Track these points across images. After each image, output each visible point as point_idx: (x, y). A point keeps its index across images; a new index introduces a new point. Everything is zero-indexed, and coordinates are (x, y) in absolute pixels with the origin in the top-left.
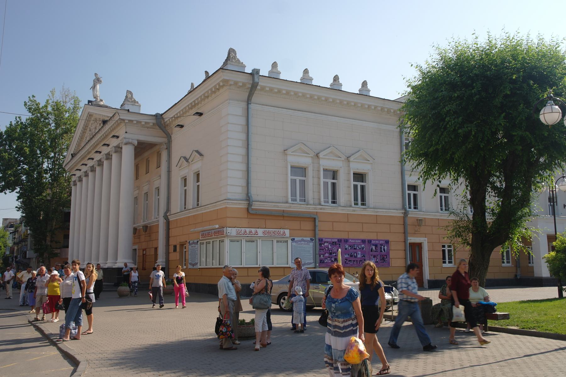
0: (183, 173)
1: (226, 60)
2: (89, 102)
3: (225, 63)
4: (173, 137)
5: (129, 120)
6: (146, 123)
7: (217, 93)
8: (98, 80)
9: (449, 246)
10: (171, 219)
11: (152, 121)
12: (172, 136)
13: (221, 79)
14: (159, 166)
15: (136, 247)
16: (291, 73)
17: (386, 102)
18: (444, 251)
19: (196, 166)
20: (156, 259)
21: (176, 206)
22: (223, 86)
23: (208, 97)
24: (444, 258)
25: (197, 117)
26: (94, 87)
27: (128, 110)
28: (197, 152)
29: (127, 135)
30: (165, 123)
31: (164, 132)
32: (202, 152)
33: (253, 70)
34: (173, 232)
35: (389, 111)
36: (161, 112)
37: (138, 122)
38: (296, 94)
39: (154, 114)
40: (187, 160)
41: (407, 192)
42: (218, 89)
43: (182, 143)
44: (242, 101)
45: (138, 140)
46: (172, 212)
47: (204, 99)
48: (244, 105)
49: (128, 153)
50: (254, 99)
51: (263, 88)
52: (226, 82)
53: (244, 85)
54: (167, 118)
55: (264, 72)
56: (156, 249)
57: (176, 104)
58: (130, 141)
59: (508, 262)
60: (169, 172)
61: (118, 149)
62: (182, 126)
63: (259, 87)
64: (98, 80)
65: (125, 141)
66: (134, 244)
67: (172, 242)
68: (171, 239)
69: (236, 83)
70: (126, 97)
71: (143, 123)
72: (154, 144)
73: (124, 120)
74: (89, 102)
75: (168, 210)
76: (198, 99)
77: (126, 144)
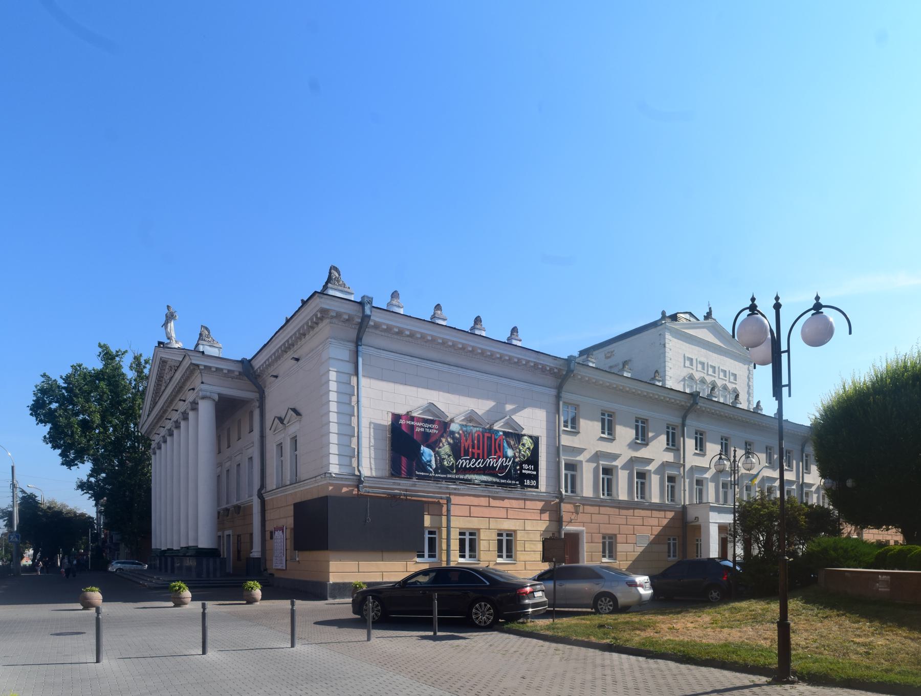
0: (279, 438)
1: (327, 283)
2: (160, 343)
3: (325, 287)
4: (267, 392)
5: (205, 366)
6: (229, 371)
7: (316, 329)
8: (170, 317)
9: (674, 539)
10: (267, 498)
11: (237, 368)
12: (266, 390)
13: (317, 308)
14: (251, 431)
15: (220, 533)
16: (415, 306)
17: (542, 357)
18: (604, 543)
19: (292, 429)
20: (252, 548)
21: (271, 483)
22: (322, 319)
23: (304, 335)
24: (604, 552)
25: (294, 362)
26: (165, 325)
27: (203, 352)
28: (294, 410)
29: (203, 386)
30: (255, 372)
31: (254, 384)
32: (301, 411)
33: (363, 297)
34: (268, 516)
35: (543, 369)
36: (249, 358)
37: (218, 370)
38: (423, 337)
39: (240, 359)
40: (281, 420)
41: (563, 472)
42: (317, 324)
43: (278, 400)
44: (348, 341)
45: (219, 394)
46: (269, 488)
47: (300, 339)
48: (352, 346)
49: (206, 410)
50: (366, 339)
51: (377, 326)
52: (324, 312)
53: (349, 320)
54: (257, 364)
55: (381, 301)
56: (251, 534)
57: (265, 345)
58: (208, 394)
59: (674, 556)
60: (262, 437)
61: (194, 406)
62: (276, 377)
63: (371, 323)
64: (170, 317)
65: (201, 394)
66: (219, 530)
67: (269, 527)
68: (267, 523)
69: (338, 315)
70: (201, 335)
71: (225, 371)
72: (243, 399)
73: (198, 366)
74: (160, 343)
75: (263, 486)
76: (291, 337)
77: (203, 398)
